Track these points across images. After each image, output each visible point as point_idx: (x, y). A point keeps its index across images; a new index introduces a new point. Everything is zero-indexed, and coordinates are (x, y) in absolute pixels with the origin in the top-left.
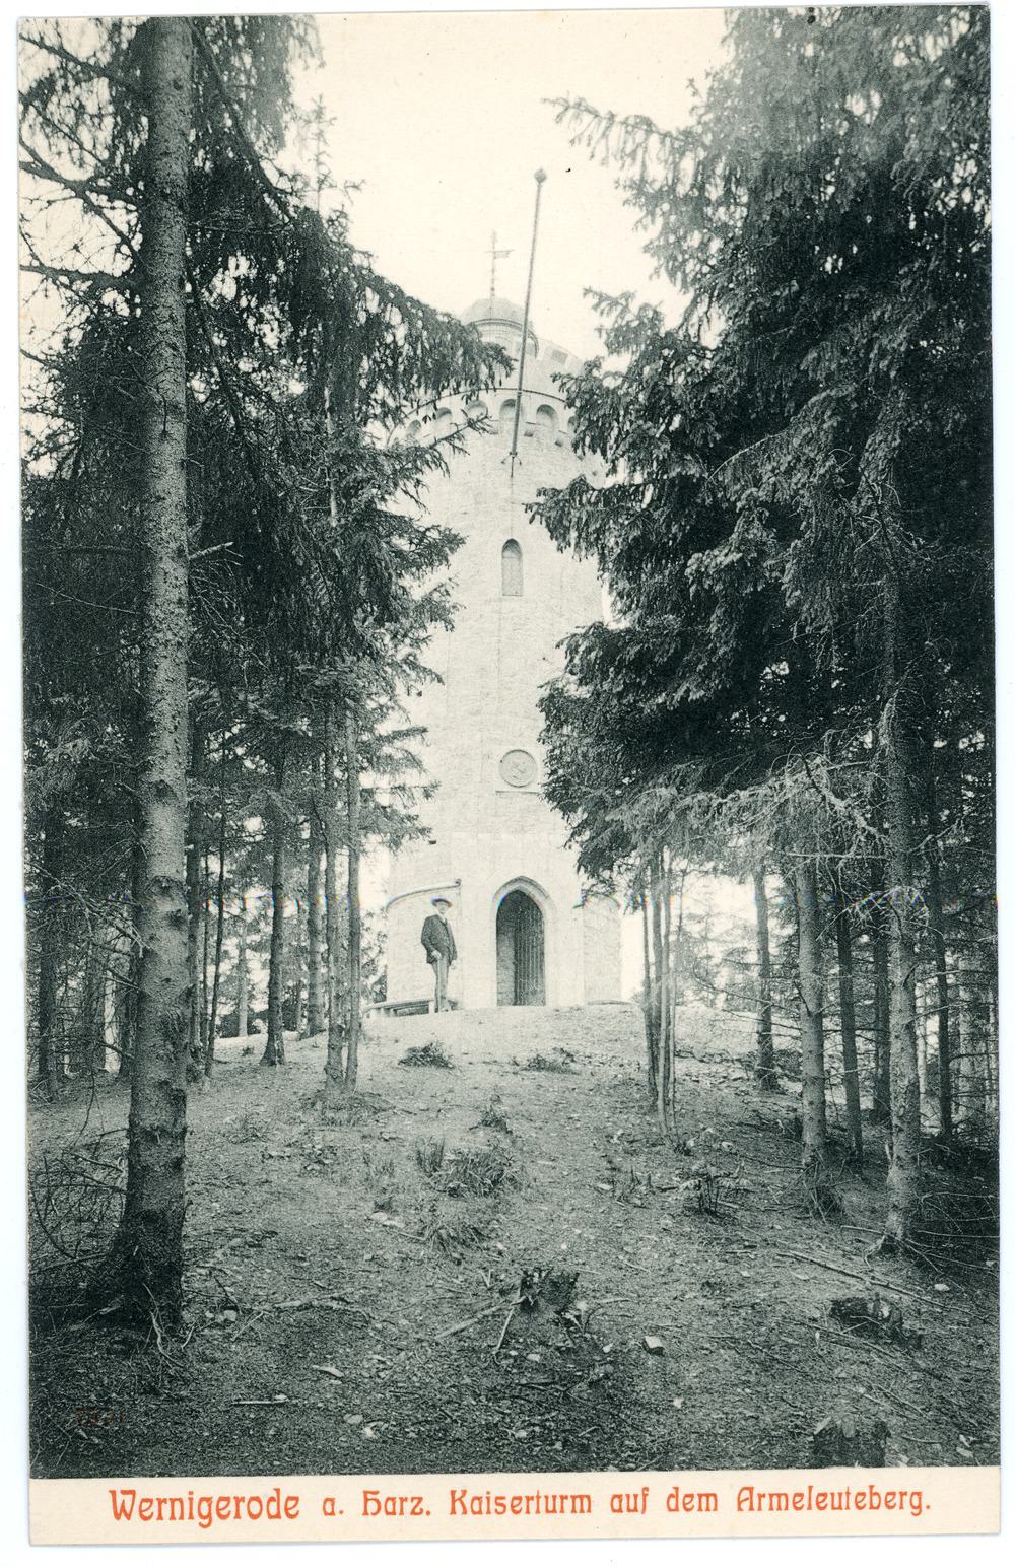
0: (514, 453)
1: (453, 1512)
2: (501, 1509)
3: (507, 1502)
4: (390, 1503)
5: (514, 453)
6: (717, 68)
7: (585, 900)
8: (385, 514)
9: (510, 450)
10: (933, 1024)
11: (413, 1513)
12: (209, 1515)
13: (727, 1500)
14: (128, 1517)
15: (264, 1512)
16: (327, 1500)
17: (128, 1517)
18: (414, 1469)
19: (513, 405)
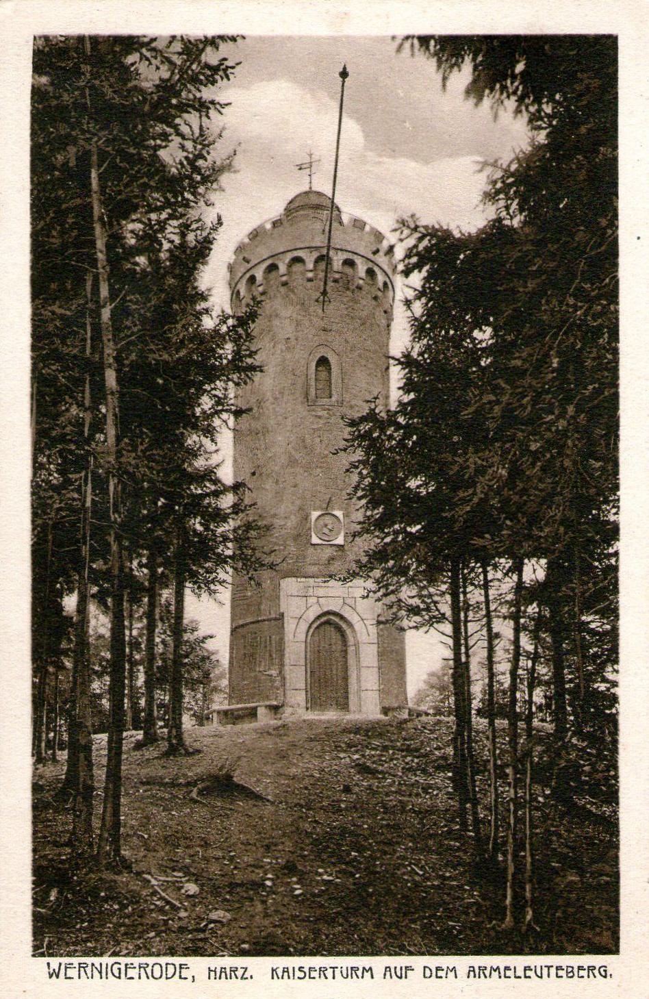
0: (324, 293)
1: (273, 978)
2: (302, 975)
3: (306, 970)
4: (170, 974)
5: (324, 293)
6: (203, 220)
7: (70, 978)
8: (468, 154)
9: (322, 290)
10: (102, 739)
11: (242, 978)
12: (221, 972)
13: (463, 971)
14: (57, 977)
15: (164, 975)
16: (386, 968)
17: (57, 977)
18: (304, 949)
19: (323, 260)
